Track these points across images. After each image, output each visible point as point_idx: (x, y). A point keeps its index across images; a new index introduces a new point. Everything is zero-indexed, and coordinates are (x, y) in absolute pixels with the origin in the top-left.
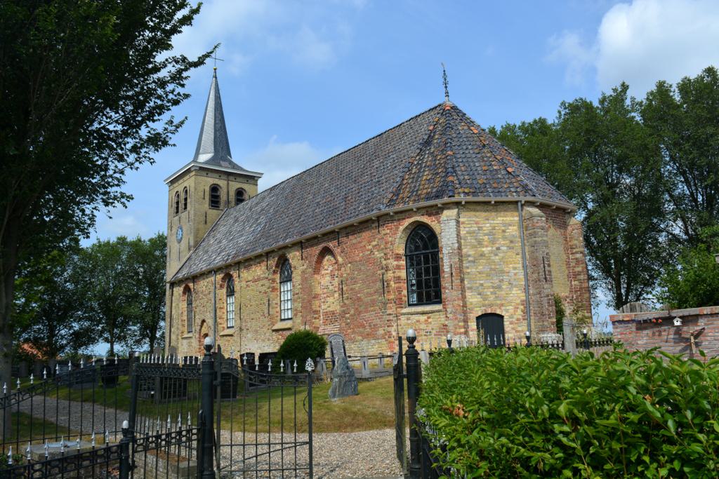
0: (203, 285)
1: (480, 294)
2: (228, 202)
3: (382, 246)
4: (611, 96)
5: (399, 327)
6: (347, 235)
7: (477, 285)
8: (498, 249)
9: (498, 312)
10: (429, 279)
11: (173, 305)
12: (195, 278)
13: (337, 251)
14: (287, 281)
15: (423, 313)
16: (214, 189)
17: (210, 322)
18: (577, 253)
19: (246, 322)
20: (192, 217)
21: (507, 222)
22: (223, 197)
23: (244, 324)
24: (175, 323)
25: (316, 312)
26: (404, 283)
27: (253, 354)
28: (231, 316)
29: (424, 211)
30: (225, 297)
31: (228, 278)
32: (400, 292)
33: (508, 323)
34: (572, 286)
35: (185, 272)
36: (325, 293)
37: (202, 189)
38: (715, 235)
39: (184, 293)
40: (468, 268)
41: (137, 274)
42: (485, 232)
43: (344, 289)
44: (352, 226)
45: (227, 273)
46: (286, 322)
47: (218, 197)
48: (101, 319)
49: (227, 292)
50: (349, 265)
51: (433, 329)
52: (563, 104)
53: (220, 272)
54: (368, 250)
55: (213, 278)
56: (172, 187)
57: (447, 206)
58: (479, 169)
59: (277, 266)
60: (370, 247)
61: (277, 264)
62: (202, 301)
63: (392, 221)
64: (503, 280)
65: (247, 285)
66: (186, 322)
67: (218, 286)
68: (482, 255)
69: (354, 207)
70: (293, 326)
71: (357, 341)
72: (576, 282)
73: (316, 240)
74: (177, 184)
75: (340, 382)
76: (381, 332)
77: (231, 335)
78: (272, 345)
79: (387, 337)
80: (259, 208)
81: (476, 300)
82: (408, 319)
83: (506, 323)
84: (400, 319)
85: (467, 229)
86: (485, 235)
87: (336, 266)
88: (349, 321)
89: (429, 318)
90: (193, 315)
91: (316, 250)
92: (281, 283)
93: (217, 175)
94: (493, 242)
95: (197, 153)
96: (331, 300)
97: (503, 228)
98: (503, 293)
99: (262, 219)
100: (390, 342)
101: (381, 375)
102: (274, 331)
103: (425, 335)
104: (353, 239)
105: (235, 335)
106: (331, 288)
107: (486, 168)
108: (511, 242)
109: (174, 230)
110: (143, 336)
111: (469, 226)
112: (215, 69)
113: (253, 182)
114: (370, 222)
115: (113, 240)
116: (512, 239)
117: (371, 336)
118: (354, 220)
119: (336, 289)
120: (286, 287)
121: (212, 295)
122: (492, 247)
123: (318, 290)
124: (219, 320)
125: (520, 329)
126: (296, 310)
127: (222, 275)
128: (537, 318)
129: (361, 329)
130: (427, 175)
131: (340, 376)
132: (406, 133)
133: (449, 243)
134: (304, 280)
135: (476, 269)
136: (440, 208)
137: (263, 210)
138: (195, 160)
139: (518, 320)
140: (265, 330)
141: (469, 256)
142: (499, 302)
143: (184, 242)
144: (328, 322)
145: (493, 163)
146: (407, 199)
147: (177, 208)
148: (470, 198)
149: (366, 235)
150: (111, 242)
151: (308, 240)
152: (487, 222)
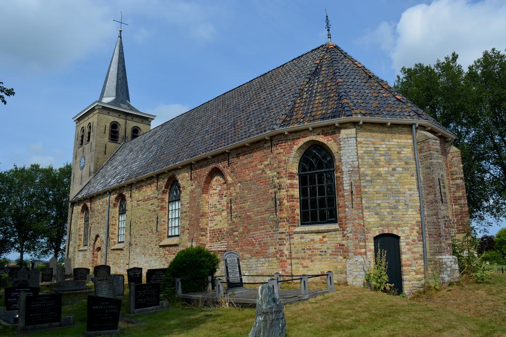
0: (99, 205)
1: (377, 214)
2: (125, 137)
3: (275, 165)
4: (444, 63)
5: (292, 246)
6: (238, 156)
7: (375, 205)
8: (394, 169)
9: (395, 232)
10: (324, 198)
11: (73, 221)
12: (92, 198)
13: (227, 171)
14: (176, 201)
15: (318, 232)
16: (114, 126)
17: (103, 237)
18: (457, 179)
19: (135, 237)
20: (93, 147)
21: (402, 144)
22: (121, 133)
24: (73, 236)
25: (204, 230)
26: (297, 202)
27: (141, 269)
28: (122, 232)
29: (320, 131)
30: (117, 214)
31: (122, 198)
32: (293, 210)
33: (405, 244)
34: (453, 209)
35: (84, 193)
36: (213, 212)
37: (104, 125)
39: (82, 211)
40: (365, 187)
41: (47, 195)
42: (381, 152)
43: (233, 207)
44: (244, 146)
45: (120, 193)
46: (173, 238)
47: (117, 132)
48: (14, 232)
49: (119, 211)
50: (239, 184)
51: (328, 249)
52: (403, 69)
53: (114, 193)
55: (107, 198)
56: (78, 124)
57: (344, 126)
58: (370, 95)
59: (166, 187)
61: (166, 185)
62: (97, 219)
63: (286, 141)
64: (399, 200)
65: (138, 205)
66: (83, 236)
67: (112, 205)
68: (379, 175)
69: (244, 130)
70: (180, 243)
71: (245, 259)
72: (457, 207)
73: (206, 162)
74: (83, 121)
75: (265, 321)
76: (272, 250)
77: (121, 250)
78: (159, 261)
79: (278, 255)
80: (151, 140)
81: (373, 220)
82: (301, 238)
83: (403, 244)
84: (293, 238)
85: (364, 149)
86: (382, 155)
88: (237, 238)
89: (324, 237)
90: (89, 230)
91: (206, 170)
92: (169, 202)
93: (117, 115)
94: (389, 162)
95: (102, 96)
96: (219, 218)
97: (398, 150)
98: (400, 213)
99: (154, 148)
100: (281, 261)
101: (289, 300)
102: (161, 246)
103: (320, 255)
104: (244, 159)
106: (219, 206)
107: (376, 95)
108: (407, 163)
109: (78, 159)
110: (50, 247)
111: (367, 146)
112: (121, 31)
113: (147, 122)
114: (263, 142)
115: (28, 167)
116: (408, 161)
117: (261, 253)
118: (245, 141)
119: (224, 208)
120: (174, 206)
121: (106, 213)
122: (388, 168)
123: (206, 209)
124: (111, 236)
125: (416, 250)
126: (184, 227)
127: (116, 196)
128: (432, 239)
129: (250, 248)
130: (318, 99)
131: (266, 313)
132: (290, 70)
133: (349, 160)
134: (192, 199)
135: (373, 188)
136: (337, 128)
137: (155, 141)
138: (100, 101)
139: (414, 241)
140: (153, 245)
141: (367, 175)
142: (395, 223)
143: (86, 169)
144: (215, 239)
145: (381, 91)
146: (302, 120)
147: (82, 141)
148: (368, 119)
149: (258, 155)
150: (26, 169)
151: (198, 162)
152: (383, 143)
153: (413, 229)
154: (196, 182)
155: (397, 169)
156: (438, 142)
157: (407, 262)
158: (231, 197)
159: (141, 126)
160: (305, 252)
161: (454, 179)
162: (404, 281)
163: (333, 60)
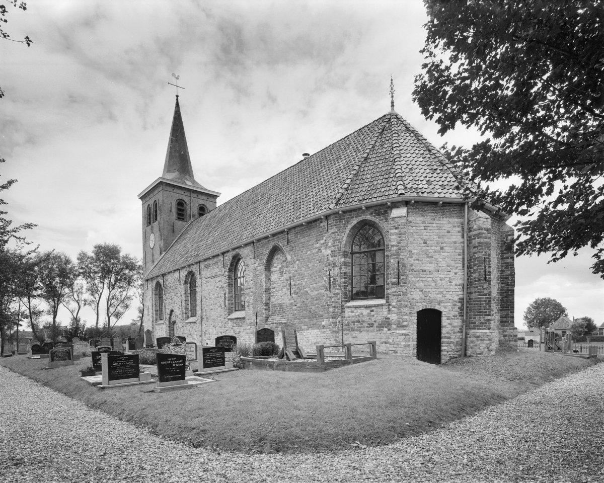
9: (437, 308)
16: (181, 203)
23: (204, 314)
38: (601, 250)
50: (297, 262)
54: (315, 249)
57: (398, 205)
60: (318, 245)
71: (302, 330)
73: (267, 240)
82: (352, 312)
87: (284, 264)
89: (372, 311)
102: (229, 319)
105: (197, 322)
136: (389, 207)
153: (456, 305)
154: (258, 260)
155: (445, 248)
156: (489, 220)
157: (446, 335)
158: (290, 274)
159: (207, 204)
160: (354, 325)
161: (504, 258)
162: (442, 351)
163: (393, 132)
